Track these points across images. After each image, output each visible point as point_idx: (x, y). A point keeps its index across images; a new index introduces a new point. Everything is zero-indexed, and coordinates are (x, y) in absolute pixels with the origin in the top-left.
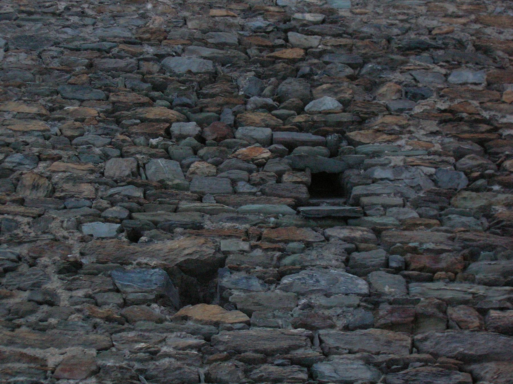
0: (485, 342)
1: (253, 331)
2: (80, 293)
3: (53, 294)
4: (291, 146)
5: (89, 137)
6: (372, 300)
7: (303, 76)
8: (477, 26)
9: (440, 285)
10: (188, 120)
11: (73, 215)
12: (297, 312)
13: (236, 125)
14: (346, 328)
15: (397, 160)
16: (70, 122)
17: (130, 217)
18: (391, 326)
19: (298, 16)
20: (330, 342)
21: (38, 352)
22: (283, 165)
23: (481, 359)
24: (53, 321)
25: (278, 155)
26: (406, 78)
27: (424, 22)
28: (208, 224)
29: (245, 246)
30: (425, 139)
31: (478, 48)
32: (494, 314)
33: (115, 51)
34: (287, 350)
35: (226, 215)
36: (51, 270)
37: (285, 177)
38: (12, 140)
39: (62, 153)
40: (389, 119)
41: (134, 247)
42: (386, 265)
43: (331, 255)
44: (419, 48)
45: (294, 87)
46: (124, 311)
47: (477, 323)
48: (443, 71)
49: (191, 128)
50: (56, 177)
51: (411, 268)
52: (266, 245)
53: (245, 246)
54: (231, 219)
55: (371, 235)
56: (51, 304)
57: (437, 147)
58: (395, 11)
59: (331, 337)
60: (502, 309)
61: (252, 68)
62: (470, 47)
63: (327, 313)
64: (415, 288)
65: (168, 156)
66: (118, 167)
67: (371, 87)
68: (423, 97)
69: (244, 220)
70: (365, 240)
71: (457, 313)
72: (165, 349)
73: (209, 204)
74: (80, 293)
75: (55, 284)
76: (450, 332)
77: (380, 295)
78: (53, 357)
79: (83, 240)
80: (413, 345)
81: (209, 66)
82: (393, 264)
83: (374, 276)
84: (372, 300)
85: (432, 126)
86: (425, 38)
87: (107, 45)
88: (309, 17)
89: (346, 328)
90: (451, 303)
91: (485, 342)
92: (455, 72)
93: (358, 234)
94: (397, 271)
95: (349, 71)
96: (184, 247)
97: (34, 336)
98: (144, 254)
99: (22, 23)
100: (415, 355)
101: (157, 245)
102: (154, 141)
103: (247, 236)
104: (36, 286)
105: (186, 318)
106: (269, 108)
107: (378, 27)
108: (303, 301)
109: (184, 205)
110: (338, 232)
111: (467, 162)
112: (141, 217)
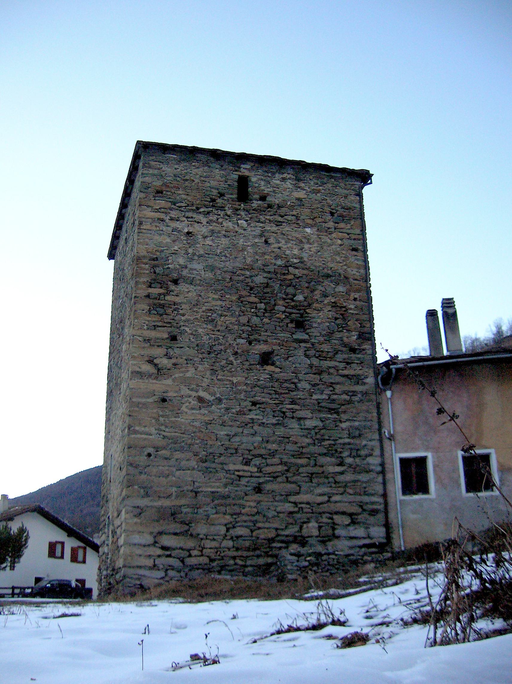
0: (338, 379)
1: (282, 374)
2: (239, 361)
3: (231, 361)
4: (291, 313)
5: (234, 308)
6: (311, 366)
7: (293, 286)
8: (345, 267)
9: (328, 362)
10: (261, 303)
11: (234, 336)
12: (292, 369)
13: (275, 305)
14: (304, 374)
15: (319, 321)
16: (228, 302)
17: (249, 338)
18: (315, 374)
19: (292, 260)
20: (301, 378)
21: (231, 379)
22: (288, 321)
23: (338, 383)
24: (233, 370)
25: (287, 317)
26: (323, 289)
27: (330, 265)
28: (269, 340)
29: (279, 348)
30: (327, 313)
31: (345, 277)
32: (340, 371)
33: (237, 273)
34: (290, 380)
35: (273, 337)
36: (230, 354)
37: (289, 325)
38: (212, 308)
39: (228, 314)
40: (317, 305)
41: (250, 347)
42: (315, 355)
43: (301, 352)
44: (328, 276)
45: (291, 290)
46: (250, 366)
47: (336, 374)
48: (334, 286)
49: (262, 306)
50: (227, 322)
51: (321, 356)
52: (285, 348)
53: (279, 348)
54: (275, 339)
55: (311, 346)
56: (232, 364)
57: (330, 316)
58: (321, 260)
59: (301, 376)
60: (343, 370)
61: (279, 282)
62: (342, 276)
63: (300, 369)
64: (322, 362)
65: (257, 316)
66: (244, 320)
67: (312, 291)
68: (327, 297)
69: (278, 339)
70: (310, 347)
71: (332, 371)
72: (261, 379)
73: (269, 334)
74: (239, 361)
75: (232, 358)
76: (329, 376)
77: (313, 364)
78: (235, 380)
79: (237, 344)
80: (320, 379)
81: (266, 281)
82: (317, 356)
83: (311, 359)
84: (311, 366)
85: (329, 308)
86: (330, 272)
87: (235, 270)
88: (295, 261)
89: (304, 374)
90: (330, 367)
91: (338, 379)
92: (337, 287)
93: (308, 346)
94: (317, 358)
95: (307, 285)
96: (264, 348)
97: (229, 374)
98: (254, 350)
99: (207, 259)
100: (321, 383)
101: (257, 347)
102: (253, 310)
103: (279, 345)
104: (227, 359)
105: (265, 370)
106: (284, 299)
107: (316, 266)
108: (294, 366)
109: (263, 334)
110: (303, 345)
111: (338, 322)
112: (252, 337)
